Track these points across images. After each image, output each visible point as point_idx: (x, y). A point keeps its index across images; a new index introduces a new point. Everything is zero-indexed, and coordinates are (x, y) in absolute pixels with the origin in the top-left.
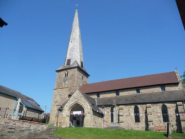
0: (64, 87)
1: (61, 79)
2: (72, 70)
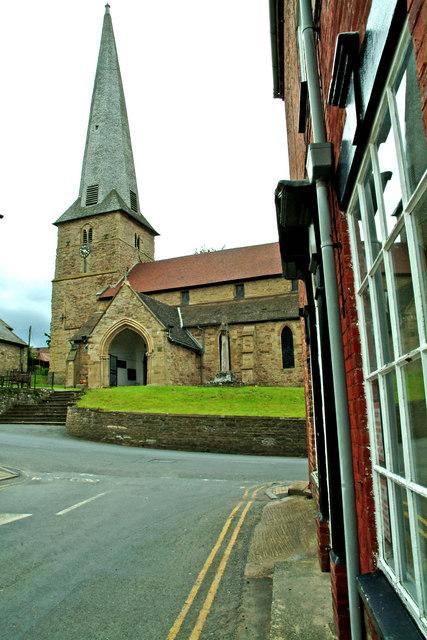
0: (83, 274)
1: (71, 249)
2: (104, 219)
